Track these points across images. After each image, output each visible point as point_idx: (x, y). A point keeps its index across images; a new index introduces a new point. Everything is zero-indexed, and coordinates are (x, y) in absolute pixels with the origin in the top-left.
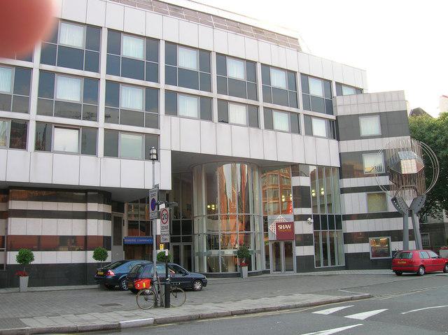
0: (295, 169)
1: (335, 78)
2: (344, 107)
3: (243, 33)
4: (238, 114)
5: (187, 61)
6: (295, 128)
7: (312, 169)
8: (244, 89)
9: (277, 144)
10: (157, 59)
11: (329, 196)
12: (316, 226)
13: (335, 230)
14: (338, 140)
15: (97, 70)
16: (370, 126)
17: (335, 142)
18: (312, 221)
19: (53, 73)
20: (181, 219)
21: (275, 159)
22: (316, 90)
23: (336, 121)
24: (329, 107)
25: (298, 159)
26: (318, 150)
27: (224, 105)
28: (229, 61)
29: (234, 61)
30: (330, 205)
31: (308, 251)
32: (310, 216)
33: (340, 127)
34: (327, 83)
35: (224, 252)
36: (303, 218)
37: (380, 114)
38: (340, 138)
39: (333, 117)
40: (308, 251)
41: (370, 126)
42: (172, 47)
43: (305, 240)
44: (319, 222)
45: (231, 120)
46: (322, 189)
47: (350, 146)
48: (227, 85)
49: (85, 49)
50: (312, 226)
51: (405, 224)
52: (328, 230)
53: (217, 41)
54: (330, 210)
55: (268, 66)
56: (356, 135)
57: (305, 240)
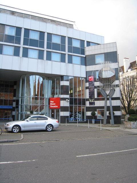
0: (62, 77)
1: (86, 39)
2: (89, 51)
3: (45, 22)
4: (56, 57)
5: (56, 40)
6: (63, 60)
7: (70, 78)
8: (39, 43)
9: (55, 67)
10: (44, 39)
11: (83, 90)
12: (71, 103)
13: (82, 105)
14: (86, 66)
15: (43, 47)
16: (100, 60)
17: (84, 67)
18: (69, 101)
19: (28, 48)
20: (73, 98)
21: (51, 73)
22: (76, 44)
23: (86, 57)
24: (83, 52)
25: (62, 74)
26: (76, 70)
27: (70, 57)
28: (73, 40)
29: (55, 36)
30: (83, 94)
31: (67, 114)
32: (68, 99)
33: (87, 60)
34: (82, 42)
35: (26, 113)
36: (64, 99)
37: (104, 53)
38: (87, 65)
39: (84, 56)
40: (67, 114)
41: (100, 60)
42: (50, 35)
43: (65, 109)
44: (72, 101)
45: (73, 62)
46: (80, 88)
47: (90, 68)
48: (72, 49)
49: (15, 36)
50: (69, 103)
51: (106, 103)
52: (78, 105)
53: (48, 28)
54: (79, 95)
55: (51, 34)
56: (93, 63)
57: (65, 109)
